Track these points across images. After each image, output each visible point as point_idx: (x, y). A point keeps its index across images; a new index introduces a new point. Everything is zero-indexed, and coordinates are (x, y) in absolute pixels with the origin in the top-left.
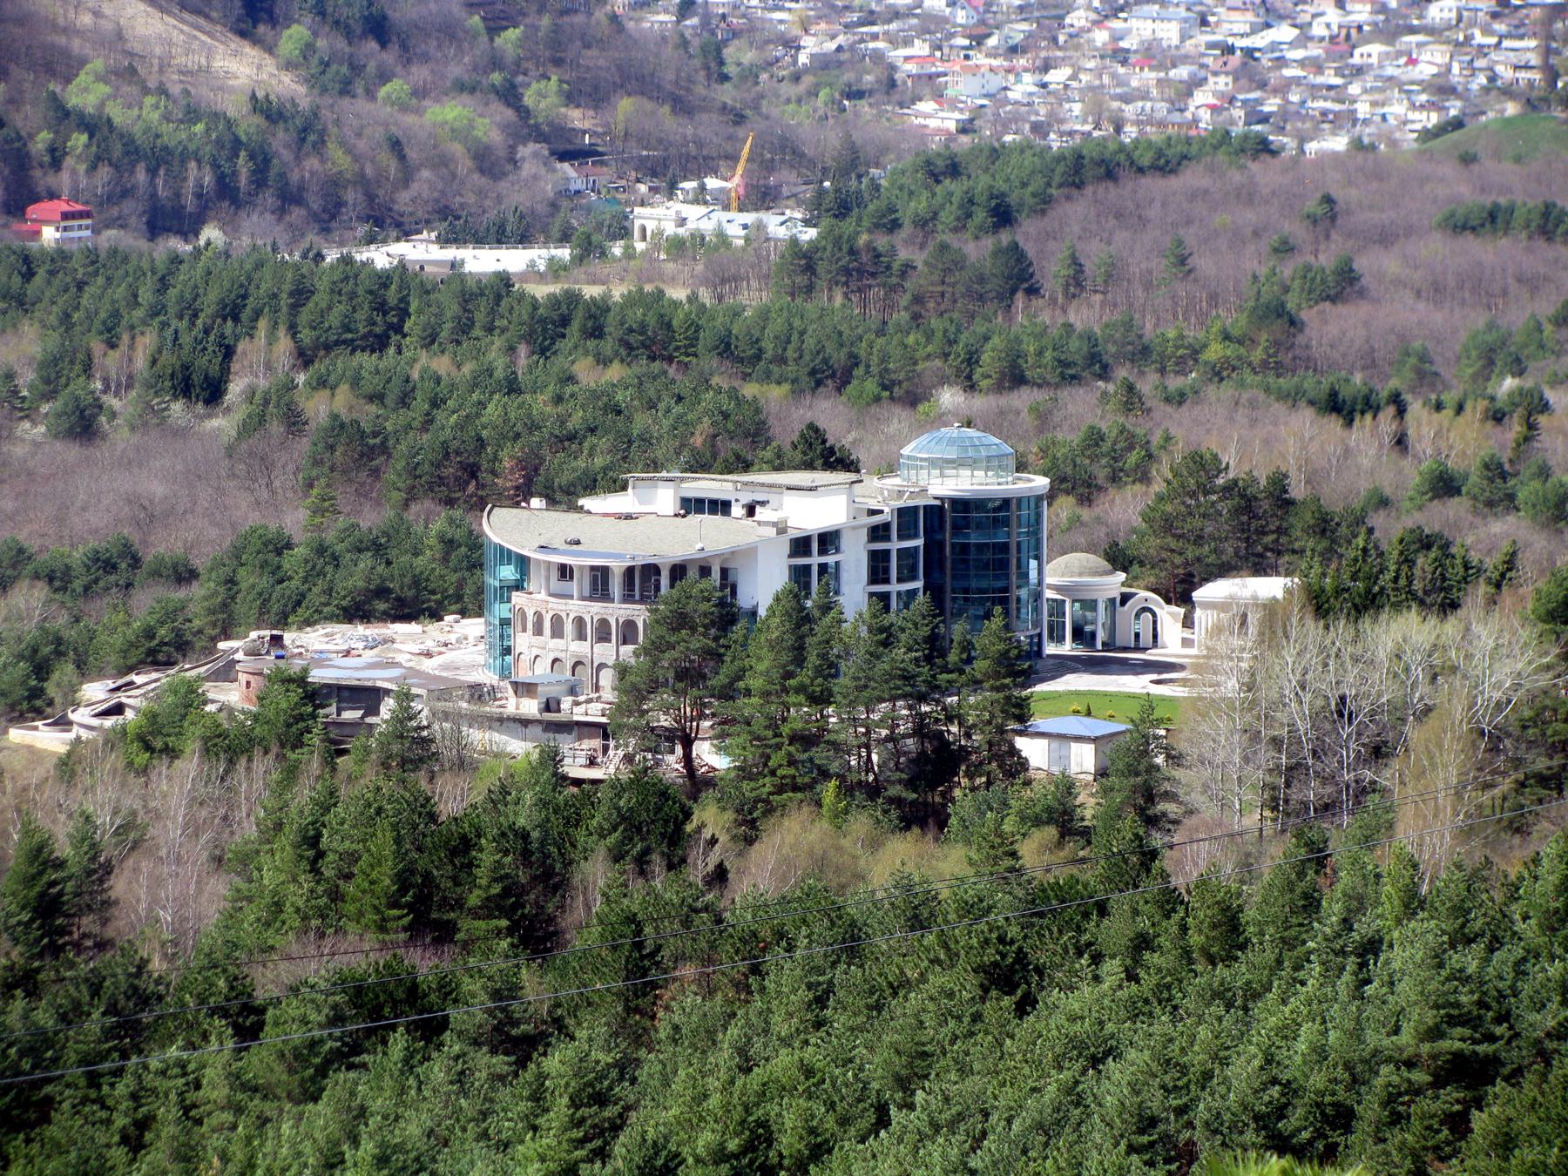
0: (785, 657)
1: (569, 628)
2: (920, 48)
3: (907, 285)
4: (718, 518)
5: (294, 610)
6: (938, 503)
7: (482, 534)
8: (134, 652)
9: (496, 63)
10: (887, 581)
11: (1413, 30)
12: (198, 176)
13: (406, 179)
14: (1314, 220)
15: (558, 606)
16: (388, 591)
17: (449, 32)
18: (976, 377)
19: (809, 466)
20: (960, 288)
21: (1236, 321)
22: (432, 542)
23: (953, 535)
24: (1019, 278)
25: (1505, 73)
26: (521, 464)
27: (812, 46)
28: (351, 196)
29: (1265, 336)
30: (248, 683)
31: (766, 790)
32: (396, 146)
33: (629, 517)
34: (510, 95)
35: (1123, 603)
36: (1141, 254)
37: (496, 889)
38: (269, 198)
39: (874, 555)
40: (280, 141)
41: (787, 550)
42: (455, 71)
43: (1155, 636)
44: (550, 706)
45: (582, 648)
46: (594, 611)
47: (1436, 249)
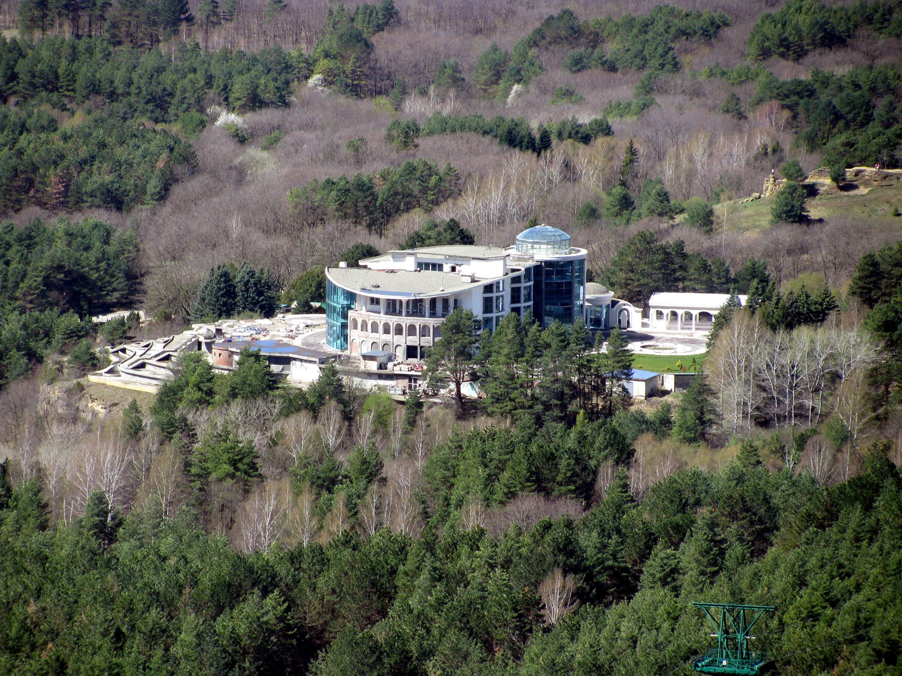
0: (516, 348)
1: (381, 328)
3: (107, 16)
4: (437, 273)
5: (22, 281)
6: (539, 263)
7: (325, 278)
8: (116, 333)
10: (519, 302)
15: (374, 317)
16: (63, 267)
18: (230, 100)
19: (452, 242)
20: (143, 18)
21: (331, 43)
22: (59, 234)
23: (546, 279)
26: (61, 180)
29: (353, 56)
30: (220, 355)
31: (509, 408)
33: (392, 271)
35: (613, 306)
37: (569, 474)
39: (513, 289)
41: (482, 290)
43: (628, 322)
44: (381, 367)
45: (388, 338)
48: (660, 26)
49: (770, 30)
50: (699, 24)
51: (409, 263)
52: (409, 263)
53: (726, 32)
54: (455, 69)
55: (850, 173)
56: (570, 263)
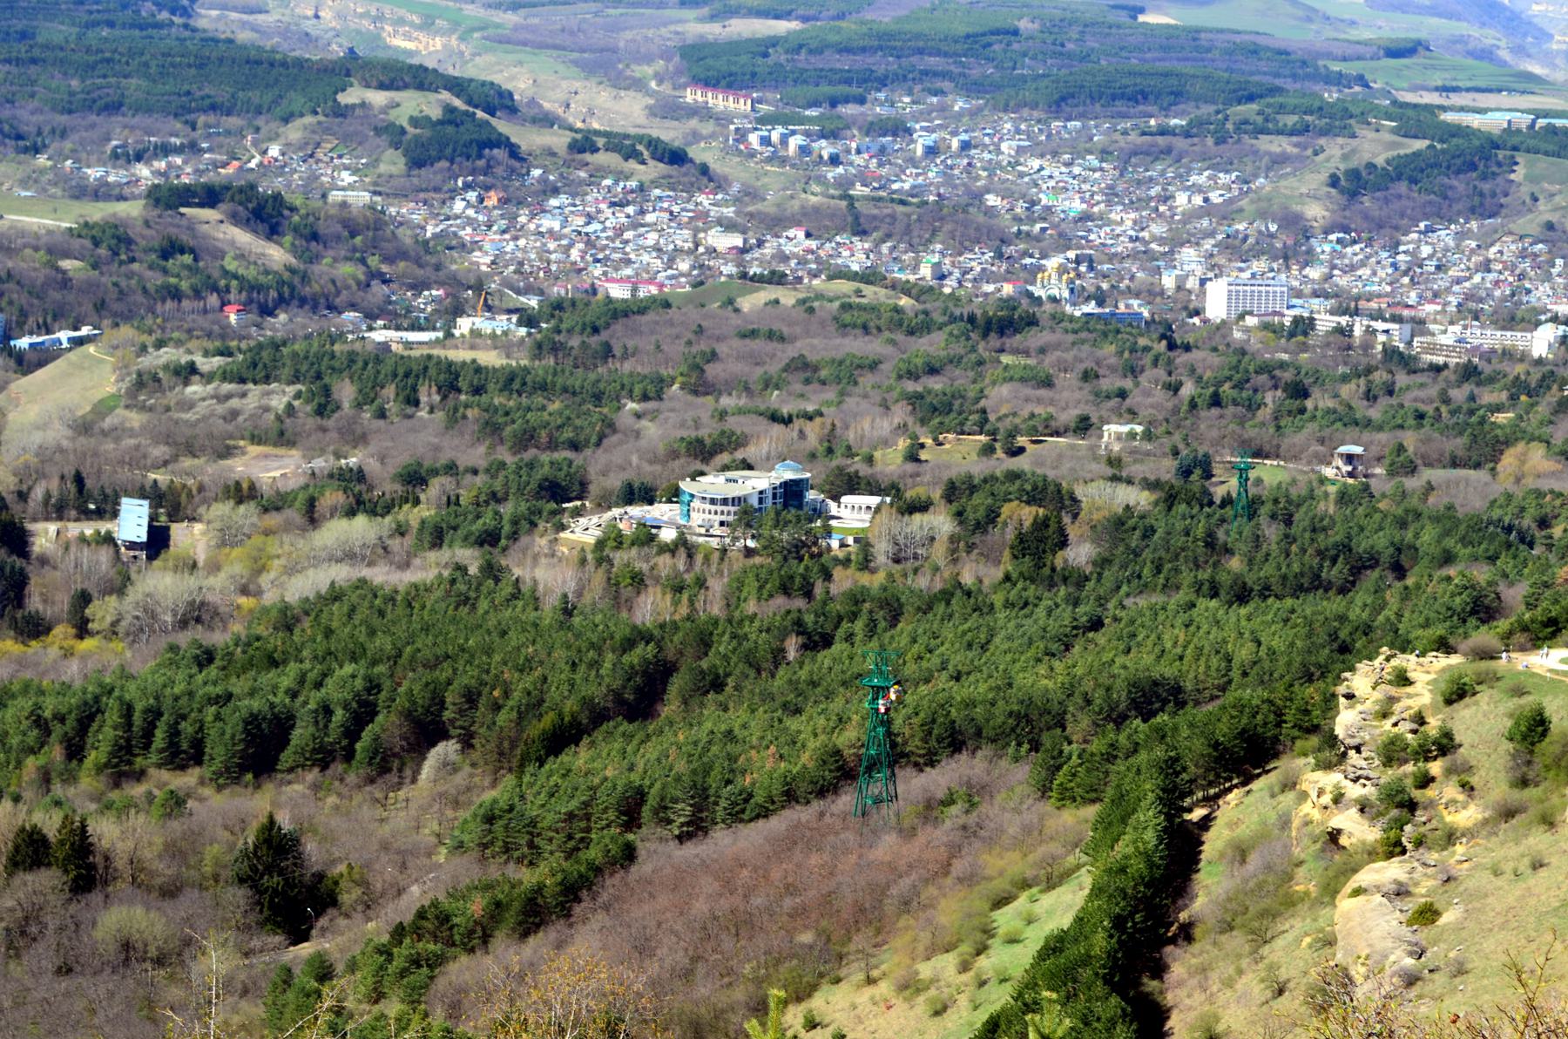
2: (469, 230)
9: (354, 250)
11: (643, 226)
12: (273, 294)
13: (338, 293)
14: (696, 333)
17: (338, 238)
21: (684, 368)
24: (607, 352)
25: (679, 243)
27: (430, 230)
28: (322, 301)
32: (333, 282)
34: (363, 261)
36: (646, 344)
38: (296, 302)
40: (296, 281)
42: (343, 253)
46: (713, 508)
47: (737, 343)
55: (941, 437)
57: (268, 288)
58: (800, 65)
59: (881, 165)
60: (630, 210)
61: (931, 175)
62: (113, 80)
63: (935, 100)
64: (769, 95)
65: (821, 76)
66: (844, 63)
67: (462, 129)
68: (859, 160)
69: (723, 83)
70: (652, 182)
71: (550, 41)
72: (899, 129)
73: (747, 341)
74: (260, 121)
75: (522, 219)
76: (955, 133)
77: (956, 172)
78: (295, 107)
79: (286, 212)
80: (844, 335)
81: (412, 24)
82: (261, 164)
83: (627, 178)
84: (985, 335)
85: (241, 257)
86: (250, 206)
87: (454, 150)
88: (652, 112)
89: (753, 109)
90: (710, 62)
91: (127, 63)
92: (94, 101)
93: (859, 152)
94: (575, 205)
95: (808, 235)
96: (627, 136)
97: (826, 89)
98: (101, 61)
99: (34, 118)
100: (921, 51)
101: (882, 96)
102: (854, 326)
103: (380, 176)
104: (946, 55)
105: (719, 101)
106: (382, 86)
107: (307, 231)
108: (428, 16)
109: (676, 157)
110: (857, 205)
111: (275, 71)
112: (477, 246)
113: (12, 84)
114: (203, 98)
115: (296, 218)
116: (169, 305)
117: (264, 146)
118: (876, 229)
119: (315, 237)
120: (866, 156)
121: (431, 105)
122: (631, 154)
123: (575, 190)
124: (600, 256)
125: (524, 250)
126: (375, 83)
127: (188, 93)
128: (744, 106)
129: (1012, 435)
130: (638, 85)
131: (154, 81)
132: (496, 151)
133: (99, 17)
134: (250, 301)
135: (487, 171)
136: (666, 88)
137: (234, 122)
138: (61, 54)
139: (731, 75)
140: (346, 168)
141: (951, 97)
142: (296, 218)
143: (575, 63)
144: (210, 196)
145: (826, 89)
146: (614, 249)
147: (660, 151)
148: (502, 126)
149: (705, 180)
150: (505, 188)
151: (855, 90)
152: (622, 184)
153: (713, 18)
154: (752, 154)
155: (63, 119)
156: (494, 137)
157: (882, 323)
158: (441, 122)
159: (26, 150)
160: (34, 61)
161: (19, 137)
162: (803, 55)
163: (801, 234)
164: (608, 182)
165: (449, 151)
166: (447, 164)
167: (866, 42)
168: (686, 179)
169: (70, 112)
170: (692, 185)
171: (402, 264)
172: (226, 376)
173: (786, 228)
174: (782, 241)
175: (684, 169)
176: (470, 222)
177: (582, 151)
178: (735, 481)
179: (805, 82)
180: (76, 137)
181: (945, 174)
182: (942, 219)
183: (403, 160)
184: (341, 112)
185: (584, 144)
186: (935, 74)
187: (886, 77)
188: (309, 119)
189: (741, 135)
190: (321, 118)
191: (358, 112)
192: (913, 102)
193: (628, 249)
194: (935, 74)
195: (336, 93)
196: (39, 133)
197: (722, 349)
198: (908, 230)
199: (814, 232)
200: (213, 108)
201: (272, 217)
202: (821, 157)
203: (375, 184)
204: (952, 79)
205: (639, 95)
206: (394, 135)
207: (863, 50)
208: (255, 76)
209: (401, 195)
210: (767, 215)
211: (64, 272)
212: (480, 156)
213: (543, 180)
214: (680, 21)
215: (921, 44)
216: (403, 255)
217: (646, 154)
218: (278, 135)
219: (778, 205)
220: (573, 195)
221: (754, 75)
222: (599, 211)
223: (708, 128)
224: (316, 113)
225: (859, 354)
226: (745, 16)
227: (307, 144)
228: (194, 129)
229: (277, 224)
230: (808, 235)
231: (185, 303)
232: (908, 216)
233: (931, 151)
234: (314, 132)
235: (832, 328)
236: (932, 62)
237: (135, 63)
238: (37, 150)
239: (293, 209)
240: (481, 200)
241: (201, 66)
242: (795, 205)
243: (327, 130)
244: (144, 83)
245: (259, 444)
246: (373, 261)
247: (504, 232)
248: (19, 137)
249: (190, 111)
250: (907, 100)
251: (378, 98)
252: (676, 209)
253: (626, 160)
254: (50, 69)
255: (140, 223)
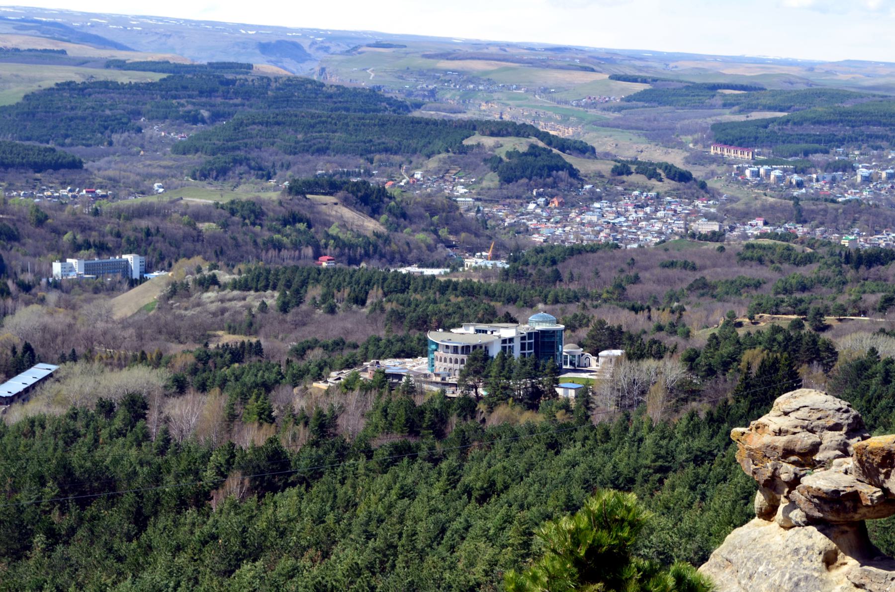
1: (448, 360)
9: (432, 224)
13: (410, 251)
14: (629, 264)
15: (445, 355)
17: (421, 217)
19: (506, 322)
25: (676, 229)
28: (397, 256)
32: (408, 244)
34: (435, 232)
36: (588, 272)
38: (377, 256)
40: (380, 242)
44: (443, 379)
46: (454, 356)
47: (658, 271)
48: (738, 282)
49: (780, 285)
50: (753, 282)
51: (472, 330)
52: (472, 330)
53: (765, 286)
54: (655, 298)
55: (757, 316)
56: (554, 332)
57: (357, 246)
58: (787, 132)
59: (831, 188)
60: (648, 209)
61: (864, 193)
62: (324, 134)
63: (875, 152)
64: (765, 150)
65: (801, 138)
66: (816, 130)
67: (539, 158)
68: (816, 185)
69: (736, 143)
70: (666, 193)
71: (633, 125)
72: (848, 167)
73: (666, 269)
74: (414, 159)
75: (573, 215)
76: (883, 169)
77: (883, 192)
78: (436, 149)
79: (386, 199)
80: (743, 265)
81: (556, 121)
82: (408, 183)
83: (649, 191)
84: (857, 267)
85: (344, 225)
86: (359, 194)
87: (532, 172)
88: (687, 161)
89: (753, 158)
90: (729, 131)
91: (336, 124)
92: (310, 147)
93: (817, 180)
94: (611, 207)
95: (766, 224)
96: (652, 164)
97: (804, 146)
98: (318, 123)
99: (272, 158)
100: (868, 123)
101: (840, 150)
102: (752, 259)
103: (482, 189)
104: (885, 125)
105: (731, 154)
106: (492, 134)
107: (398, 212)
108: (565, 116)
109: (683, 177)
110: (800, 203)
111: (428, 128)
112: (537, 230)
113: (261, 137)
114: (379, 144)
115: (393, 203)
116: (272, 253)
117: (412, 172)
118: (813, 219)
119: (404, 216)
120: (822, 183)
121: (521, 145)
122: (653, 175)
123: (613, 198)
124: (619, 237)
125: (569, 233)
126: (488, 132)
127: (371, 141)
128: (747, 156)
129: (819, 314)
130: (681, 145)
131: (351, 135)
132: (560, 172)
133: (339, 105)
134: (342, 254)
135: (554, 185)
136: (699, 148)
137: (397, 158)
138: (294, 119)
139: (741, 138)
140: (462, 184)
141: (886, 151)
142: (393, 203)
143: (645, 135)
144: (332, 187)
145: (804, 146)
146: (630, 233)
147: (673, 173)
148: (569, 159)
149: (703, 192)
150: (564, 197)
151: (822, 146)
152: (645, 194)
153: (741, 112)
154: (746, 182)
155: (290, 158)
156: (560, 164)
157: (775, 258)
158: (525, 154)
159: (262, 177)
160: (278, 123)
161: (260, 169)
162: (790, 126)
163: (760, 223)
164: (636, 193)
165: (528, 172)
166: (527, 181)
167: (832, 117)
168: (689, 191)
169: (295, 154)
170: (693, 194)
171: (463, 235)
172: (235, 286)
173: (751, 219)
174: (747, 227)
175: (688, 184)
176: (537, 217)
177: (621, 173)
178: (485, 332)
179: (790, 142)
180: (295, 168)
181: (875, 193)
182: (860, 212)
183: (498, 178)
184: (464, 150)
185: (622, 170)
186: (877, 137)
187: (844, 139)
188: (443, 155)
189: (741, 171)
190: (451, 154)
191: (475, 150)
192: (861, 154)
193: (639, 233)
194: (877, 137)
195: (463, 139)
196: (274, 166)
197: (644, 275)
198: (835, 219)
199: (770, 221)
200: (387, 150)
201: (375, 202)
202: (791, 183)
203: (479, 194)
204: (888, 140)
205: (681, 151)
206: (495, 163)
207: (830, 122)
208: (415, 131)
209: (493, 201)
210: (738, 210)
211: (201, 231)
212: (549, 176)
213: (591, 191)
214: (720, 114)
215: (868, 118)
216: (466, 229)
217: (663, 175)
218: (422, 165)
219: (746, 204)
220: (611, 201)
221: (756, 138)
222: (627, 211)
223: (720, 170)
224: (448, 152)
225: (748, 277)
226: (761, 110)
227: (440, 170)
228: (372, 163)
229: (379, 207)
230: (766, 224)
231: (284, 253)
232: (837, 210)
233: (867, 180)
234: (445, 163)
235: (735, 261)
236: (875, 129)
237: (340, 124)
238: (269, 178)
239: (391, 198)
240: (547, 203)
241: (383, 125)
242: (758, 204)
243: (454, 162)
244: (344, 135)
245: (234, 333)
246: (443, 232)
247: (557, 222)
248: (260, 169)
249: (370, 152)
250: (857, 153)
251: (489, 142)
252: (679, 209)
253: (650, 178)
254: (287, 128)
255: (276, 203)
